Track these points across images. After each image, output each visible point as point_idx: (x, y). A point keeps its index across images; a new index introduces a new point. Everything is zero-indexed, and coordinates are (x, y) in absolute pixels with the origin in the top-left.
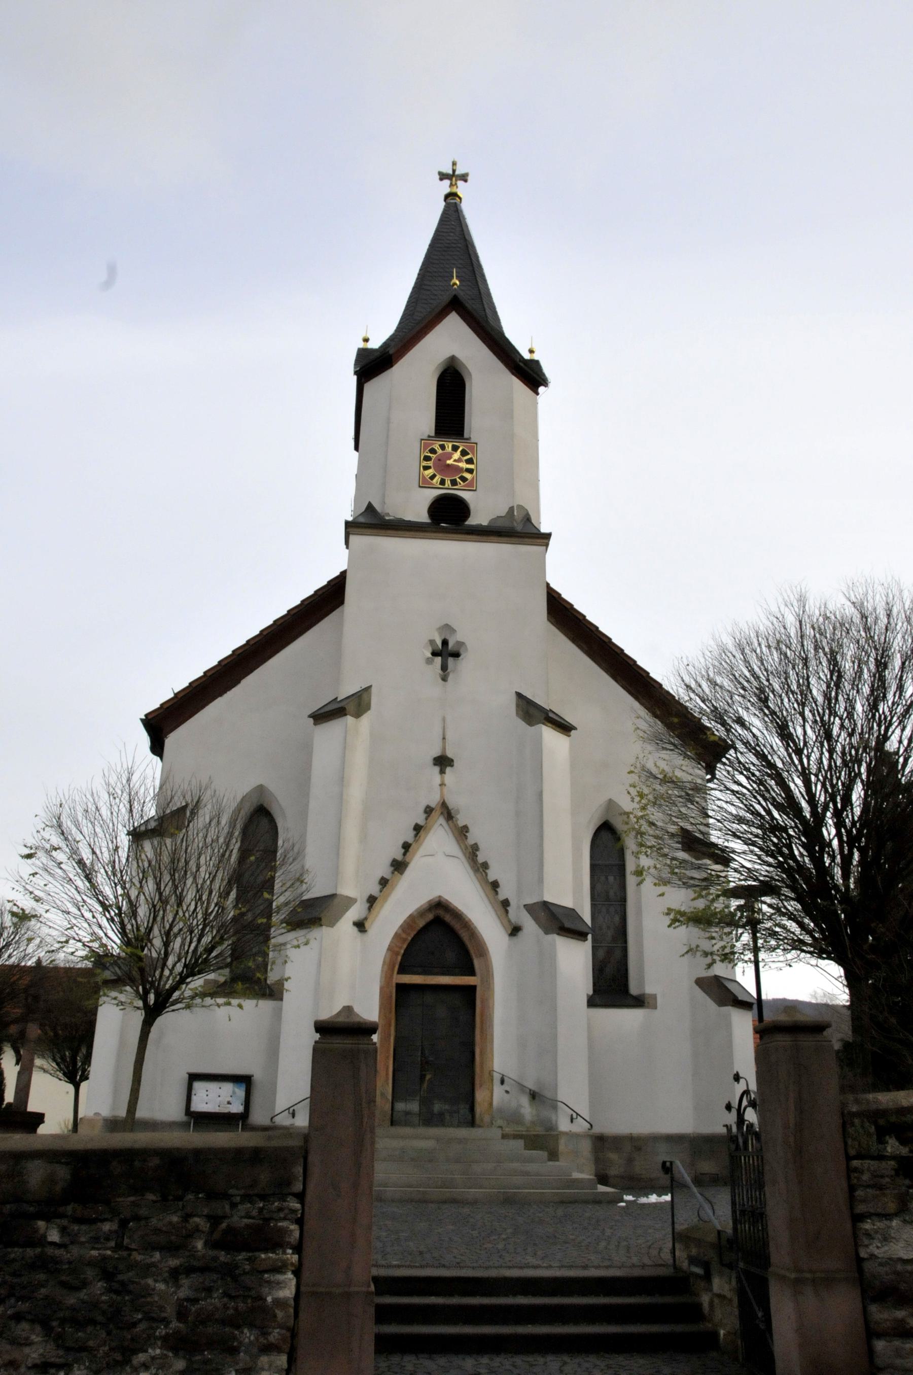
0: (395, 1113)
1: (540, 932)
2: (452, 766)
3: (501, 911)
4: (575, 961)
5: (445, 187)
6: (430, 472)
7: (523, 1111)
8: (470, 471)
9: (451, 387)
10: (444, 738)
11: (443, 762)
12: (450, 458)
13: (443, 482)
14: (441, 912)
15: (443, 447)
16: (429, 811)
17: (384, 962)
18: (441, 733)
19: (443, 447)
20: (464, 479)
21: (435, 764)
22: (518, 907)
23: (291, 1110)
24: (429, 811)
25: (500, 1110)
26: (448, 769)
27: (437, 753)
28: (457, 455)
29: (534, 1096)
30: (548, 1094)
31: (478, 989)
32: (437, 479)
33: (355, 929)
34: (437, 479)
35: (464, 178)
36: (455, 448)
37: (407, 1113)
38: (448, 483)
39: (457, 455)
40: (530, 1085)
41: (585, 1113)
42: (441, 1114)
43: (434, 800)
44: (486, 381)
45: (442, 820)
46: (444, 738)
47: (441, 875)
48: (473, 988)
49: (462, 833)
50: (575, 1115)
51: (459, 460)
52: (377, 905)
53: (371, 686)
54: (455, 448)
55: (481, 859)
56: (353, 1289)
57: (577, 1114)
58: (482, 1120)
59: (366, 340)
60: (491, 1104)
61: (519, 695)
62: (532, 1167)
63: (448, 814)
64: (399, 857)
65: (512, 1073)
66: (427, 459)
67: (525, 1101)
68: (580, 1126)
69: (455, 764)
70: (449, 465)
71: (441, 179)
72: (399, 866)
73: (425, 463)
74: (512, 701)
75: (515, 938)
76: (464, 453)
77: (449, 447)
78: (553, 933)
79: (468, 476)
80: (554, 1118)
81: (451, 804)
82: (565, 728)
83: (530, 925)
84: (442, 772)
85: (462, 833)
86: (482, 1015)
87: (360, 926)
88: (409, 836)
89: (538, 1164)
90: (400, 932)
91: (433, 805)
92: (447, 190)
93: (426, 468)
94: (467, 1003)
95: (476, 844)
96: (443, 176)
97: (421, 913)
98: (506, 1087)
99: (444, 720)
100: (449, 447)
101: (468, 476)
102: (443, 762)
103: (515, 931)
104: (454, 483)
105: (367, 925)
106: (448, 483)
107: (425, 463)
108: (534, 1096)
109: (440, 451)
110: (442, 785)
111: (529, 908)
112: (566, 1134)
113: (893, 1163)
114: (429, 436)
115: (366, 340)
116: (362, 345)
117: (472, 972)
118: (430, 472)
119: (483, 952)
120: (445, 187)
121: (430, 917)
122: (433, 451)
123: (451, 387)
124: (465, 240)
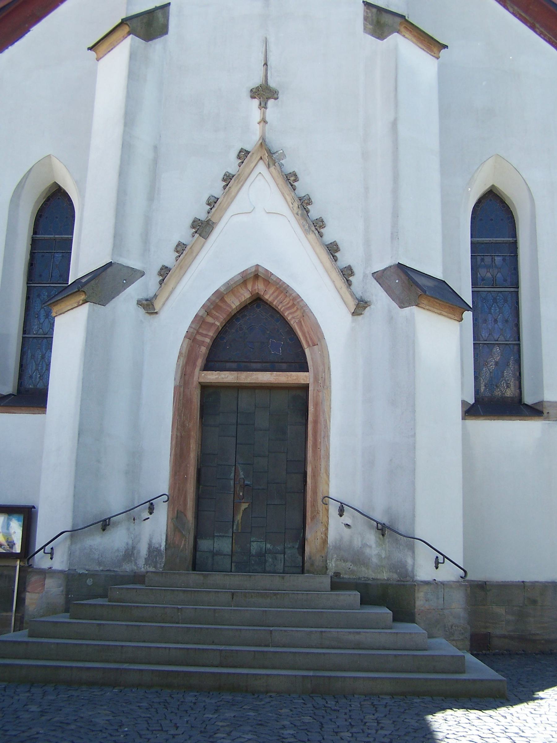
0: (198, 554)
1: (394, 305)
2: (276, 99)
3: (340, 282)
4: (443, 346)
7: (367, 551)
10: (266, 64)
11: (264, 93)
14: (260, 287)
16: (243, 155)
17: (180, 353)
18: (262, 57)
21: (253, 97)
22: (365, 276)
23: (48, 549)
24: (243, 155)
25: (338, 548)
26: (271, 102)
27: (256, 81)
29: (383, 529)
30: (402, 529)
31: (311, 389)
33: (141, 311)
37: (215, 554)
40: (379, 516)
41: (456, 552)
42: (261, 555)
43: (251, 142)
45: (261, 168)
46: (266, 64)
47: (261, 236)
48: (305, 388)
49: (290, 180)
50: (441, 558)
52: (171, 280)
53: (169, 4)
55: (314, 213)
57: (445, 557)
58: (312, 565)
60: (325, 541)
62: (367, 636)
63: (269, 154)
64: (203, 216)
65: (356, 500)
67: (371, 538)
68: (448, 573)
69: (280, 96)
72: (202, 228)
75: (360, 318)
78: (410, 305)
80: (410, 561)
81: (275, 146)
82: (432, 45)
83: (380, 298)
84: (263, 106)
85: (290, 180)
86: (316, 422)
87: (148, 306)
88: (217, 190)
89: (379, 628)
90: (203, 313)
91: (248, 148)
94: (297, 409)
97: (231, 288)
98: (347, 519)
99: (266, 42)
102: (264, 93)
103: (361, 306)
105: (157, 305)
108: (383, 529)
110: (264, 121)
111: (379, 277)
112: (427, 583)
113: (136, 568)
117: (304, 368)
119: (318, 338)
121: (245, 295)
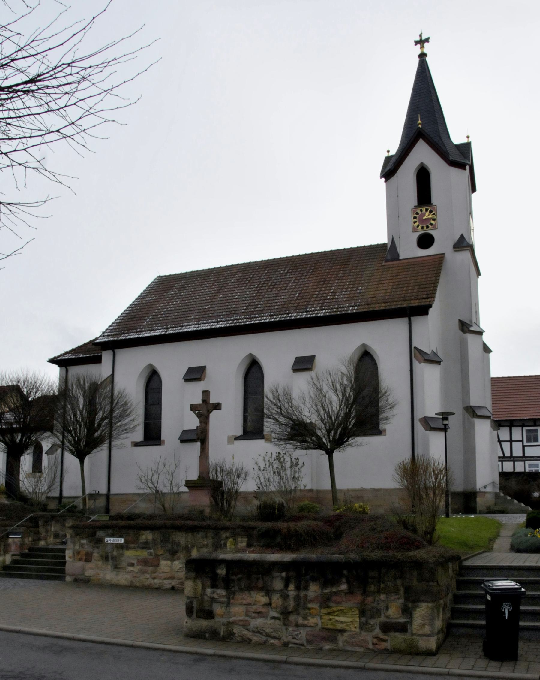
5: (418, 50)
6: (416, 224)
8: (434, 220)
9: (423, 176)
12: (425, 215)
13: (422, 228)
15: (421, 211)
19: (421, 211)
20: (431, 224)
23: (419, 427)
28: (427, 213)
32: (420, 227)
34: (420, 227)
35: (427, 40)
36: (427, 210)
38: (425, 228)
39: (427, 213)
44: (442, 175)
51: (429, 215)
54: (427, 210)
56: (232, 619)
59: (388, 151)
61: (460, 321)
66: (415, 218)
70: (425, 219)
71: (416, 45)
73: (414, 220)
74: (457, 323)
76: (431, 212)
77: (424, 210)
79: (433, 222)
92: (419, 52)
93: (415, 222)
95: (487, 507)
96: (417, 43)
100: (424, 210)
101: (433, 222)
104: (427, 227)
106: (425, 228)
107: (414, 220)
109: (420, 213)
114: (415, 206)
115: (388, 151)
116: (386, 155)
118: (416, 224)
120: (418, 50)
122: (417, 214)
123: (423, 176)
124: (432, 100)
